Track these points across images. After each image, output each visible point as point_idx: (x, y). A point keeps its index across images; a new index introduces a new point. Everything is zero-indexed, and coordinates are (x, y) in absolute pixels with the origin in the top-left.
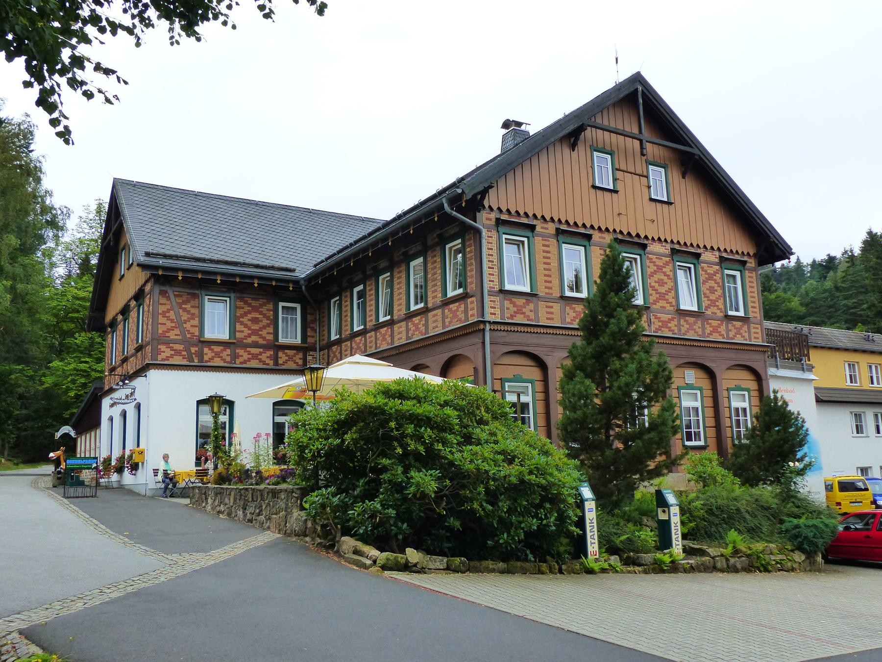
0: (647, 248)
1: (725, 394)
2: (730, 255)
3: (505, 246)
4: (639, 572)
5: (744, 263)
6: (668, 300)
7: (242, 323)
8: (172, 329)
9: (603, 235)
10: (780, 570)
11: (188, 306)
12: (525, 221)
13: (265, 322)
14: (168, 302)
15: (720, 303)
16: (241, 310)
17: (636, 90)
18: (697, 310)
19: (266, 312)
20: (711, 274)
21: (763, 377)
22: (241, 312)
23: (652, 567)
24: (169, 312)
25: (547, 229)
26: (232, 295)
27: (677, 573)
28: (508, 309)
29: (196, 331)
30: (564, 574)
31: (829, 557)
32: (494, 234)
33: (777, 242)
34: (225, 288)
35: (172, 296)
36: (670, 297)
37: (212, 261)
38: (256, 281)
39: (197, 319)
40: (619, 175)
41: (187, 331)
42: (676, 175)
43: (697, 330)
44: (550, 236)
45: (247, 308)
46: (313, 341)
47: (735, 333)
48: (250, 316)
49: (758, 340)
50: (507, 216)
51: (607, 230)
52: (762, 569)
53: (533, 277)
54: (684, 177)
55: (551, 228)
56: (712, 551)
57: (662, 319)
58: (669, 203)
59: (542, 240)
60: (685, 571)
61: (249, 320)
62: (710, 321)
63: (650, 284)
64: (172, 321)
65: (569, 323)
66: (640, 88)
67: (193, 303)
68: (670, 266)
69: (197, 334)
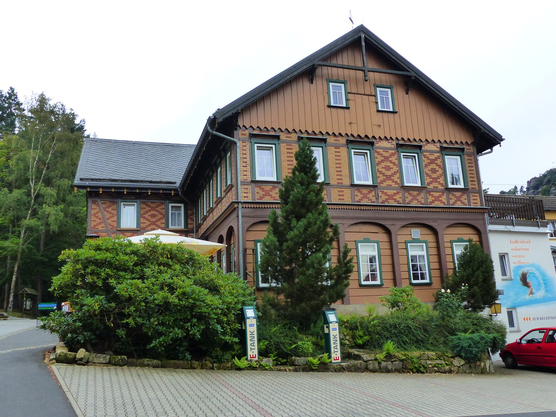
0: (422, 148)
1: (449, 245)
2: (450, 145)
3: (256, 151)
4: (290, 370)
5: (462, 150)
6: (394, 180)
7: (144, 218)
8: (100, 223)
9: (338, 139)
10: (436, 372)
11: (110, 209)
12: (273, 133)
13: (160, 216)
14: (98, 208)
15: (441, 180)
16: (144, 210)
17: (360, 37)
18: (420, 186)
19: (160, 210)
20: (433, 160)
21: (482, 231)
22: (144, 211)
23: (302, 367)
24: (98, 214)
25: (291, 137)
26: (138, 201)
27: (328, 371)
28: (258, 193)
29: (115, 224)
30: (214, 369)
31: (519, 365)
32: (248, 144)
33: (488, 132)
34: (133, 197)
35: (100, 203)
36: (396, 178)
37: (122, 181)
38: (173, 192)
39: (116, 217)
40: (351, 96)
41: (109, 224)
42: (400, 92)
43: (463, 201)
44: (293, 142)
45: (148, 209)
46: (192, 227)
47: (455, 201)
48: (150, 213)
49: (477, 205)
50: (258, 131)
51: (340, 134)
52: (415, 370)
53: (278, 171)
54: (407, 93)
55: (343, 141)
56: (365, 357)
57: (388, 194)
58: (394, 112)
59: (287, 145)
60: (336, 371)
61: (149, 216)
62: (432, 193)
63: (378, 169)
64: (100, 219)
65: (357, 202)
66: (363, 36)
67: (113, 207)
68: (396, 156)
69: (115, 226)
